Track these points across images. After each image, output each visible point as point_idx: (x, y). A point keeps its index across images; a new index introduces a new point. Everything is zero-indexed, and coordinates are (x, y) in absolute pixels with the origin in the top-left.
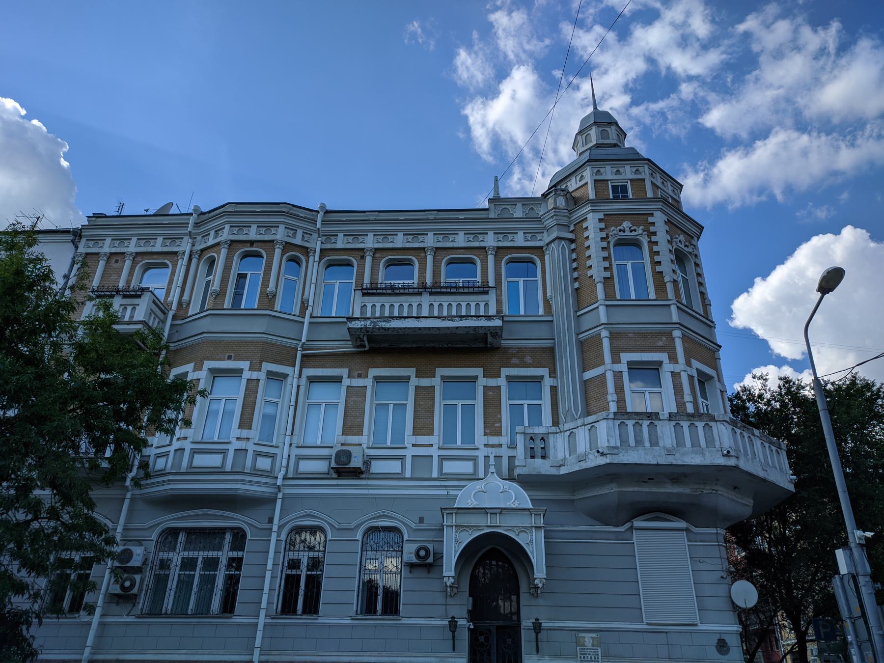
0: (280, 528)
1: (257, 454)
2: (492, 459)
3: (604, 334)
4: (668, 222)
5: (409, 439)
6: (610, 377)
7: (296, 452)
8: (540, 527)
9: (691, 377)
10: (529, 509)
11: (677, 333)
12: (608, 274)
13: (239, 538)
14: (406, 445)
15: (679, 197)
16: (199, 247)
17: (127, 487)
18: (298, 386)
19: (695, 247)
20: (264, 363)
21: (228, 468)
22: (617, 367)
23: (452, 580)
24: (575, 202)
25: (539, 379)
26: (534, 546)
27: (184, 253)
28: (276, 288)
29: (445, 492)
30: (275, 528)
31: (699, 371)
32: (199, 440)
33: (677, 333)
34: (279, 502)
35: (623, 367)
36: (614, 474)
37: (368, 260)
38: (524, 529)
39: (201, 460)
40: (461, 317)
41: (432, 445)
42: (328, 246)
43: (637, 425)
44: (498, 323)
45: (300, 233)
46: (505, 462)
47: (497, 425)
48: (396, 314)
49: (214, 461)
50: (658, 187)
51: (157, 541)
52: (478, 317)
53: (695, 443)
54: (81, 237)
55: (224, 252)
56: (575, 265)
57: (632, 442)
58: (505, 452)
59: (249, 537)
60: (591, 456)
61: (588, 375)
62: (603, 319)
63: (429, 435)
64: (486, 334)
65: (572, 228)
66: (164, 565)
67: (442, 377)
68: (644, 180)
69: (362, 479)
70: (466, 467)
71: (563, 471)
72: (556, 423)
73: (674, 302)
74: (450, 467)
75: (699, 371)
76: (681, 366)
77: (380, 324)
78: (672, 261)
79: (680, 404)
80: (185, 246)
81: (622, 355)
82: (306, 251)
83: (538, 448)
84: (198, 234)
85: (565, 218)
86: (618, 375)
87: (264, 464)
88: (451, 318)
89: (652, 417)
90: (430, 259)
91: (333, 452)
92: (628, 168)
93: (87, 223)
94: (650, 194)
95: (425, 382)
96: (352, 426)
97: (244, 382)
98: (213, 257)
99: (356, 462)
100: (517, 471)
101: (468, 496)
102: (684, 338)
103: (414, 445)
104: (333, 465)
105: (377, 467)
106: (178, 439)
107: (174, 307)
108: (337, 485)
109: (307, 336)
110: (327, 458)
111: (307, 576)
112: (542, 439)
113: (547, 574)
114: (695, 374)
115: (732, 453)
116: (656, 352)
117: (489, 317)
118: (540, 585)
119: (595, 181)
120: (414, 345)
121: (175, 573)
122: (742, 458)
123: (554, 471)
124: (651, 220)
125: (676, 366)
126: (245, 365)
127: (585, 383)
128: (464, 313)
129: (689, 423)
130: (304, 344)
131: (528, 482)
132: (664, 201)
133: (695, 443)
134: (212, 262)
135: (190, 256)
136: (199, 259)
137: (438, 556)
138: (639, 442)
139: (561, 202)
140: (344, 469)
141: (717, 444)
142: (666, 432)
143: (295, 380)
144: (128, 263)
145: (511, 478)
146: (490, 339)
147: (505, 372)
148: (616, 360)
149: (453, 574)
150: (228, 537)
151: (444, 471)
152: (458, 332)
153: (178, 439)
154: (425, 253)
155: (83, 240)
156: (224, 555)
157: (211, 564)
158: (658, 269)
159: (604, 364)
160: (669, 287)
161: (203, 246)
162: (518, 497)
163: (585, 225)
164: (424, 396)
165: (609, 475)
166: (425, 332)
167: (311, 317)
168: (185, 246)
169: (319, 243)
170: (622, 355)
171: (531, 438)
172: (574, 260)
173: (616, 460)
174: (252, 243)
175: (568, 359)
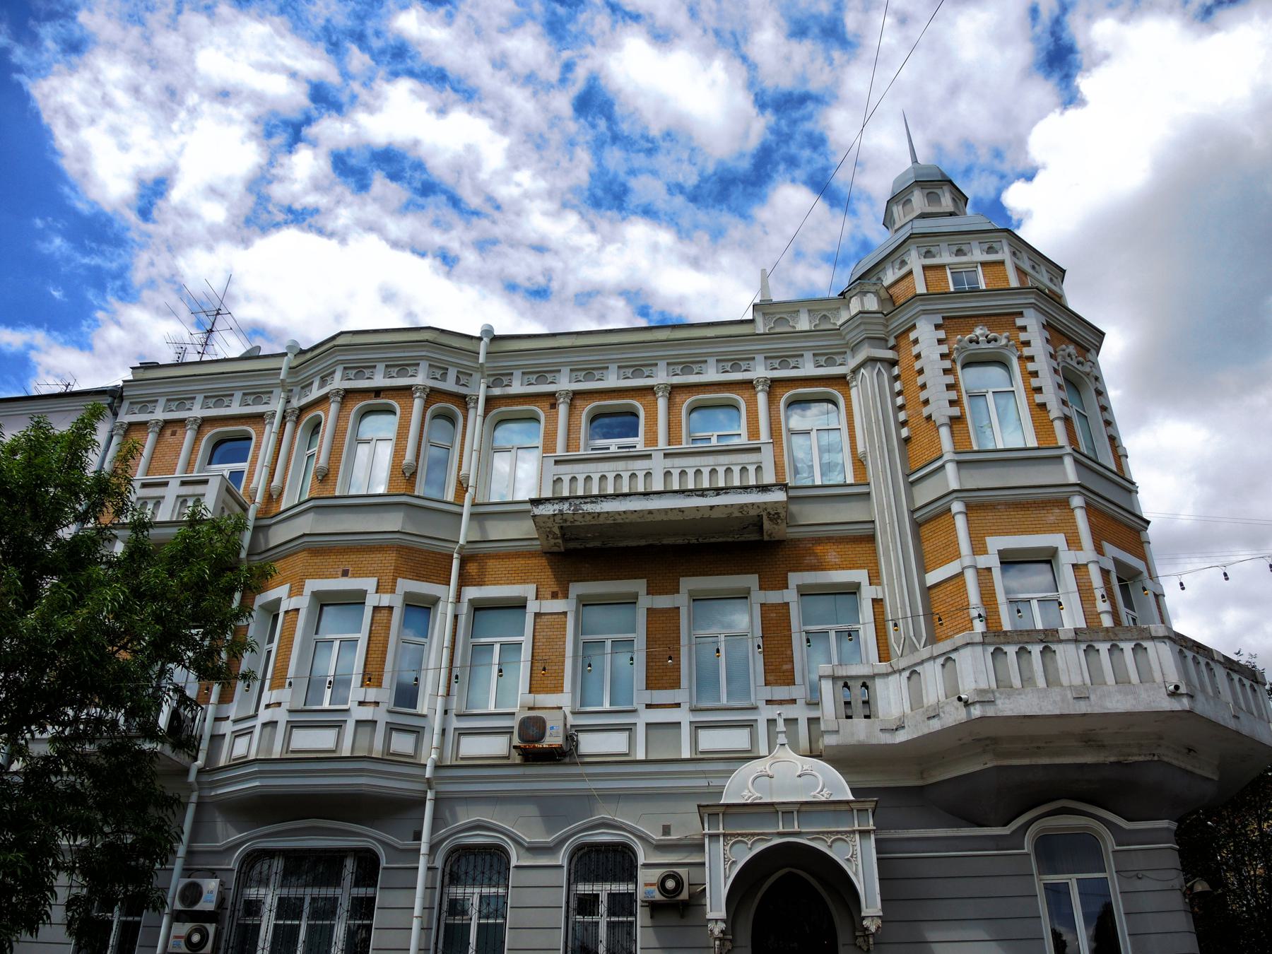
0: (433, 848)
1: (392, 728)
2: (781, 726)
3: (957, 507)
4: (1047, 326)
5: (642, 696)
6: (970, 576)
7: (455, 723)
8: (868, 832)
9: (1105, 573)
10: (848, 802)
11: (1077, 501)
12: (955, 411)
13: (368, 868)
14: (635, 706)
15: (1061, 289)
16: (296, 403)
17: (190, 784)
18: (456, 617)
19: (1095, 364)
20: (399, 580)
21: (346, 752)
22: (982, 562)
23: (723, 926)
24: (891, 304)
25: (852, 590)
26: (860, 862)
27: (274, 414)
28: (417, 461)
29: (704, 783)
30: (424, 848)
31: (1115, 560)
32: (301, 706)
33: (1077, 501)
34: (429, 807)
35: (992, 561)
36: (987, 738)
37: (562, 409)
38: (840, 837)
39: (307, 740)
40: (718, 491)
41: (678, 705)
42: (497, 391)
43: (1022, 652)
44: (780, 496)
45: (452, 373)
46: (803, 727)
47: (785, 667)
48: (610, 491)
49: (321, 740)
50: (1026, 274)
51: (239, 872)
52: (745, 488)
53: (1121, 679)
54: (121, 398)
55: (334, 408)
56: (900, 401)
57: (1017, 682)
58: (801, 713)
59: (383, 863)
60: (947, 708)
61: (932, 578)
62: (954, 485)
63: (673, 688)
64: (760, 517)
65: (892, 342)
66: (253, 908)
67: (691, 593)
68: (1002, 263)
69: (565, 764)
70: (737, 740)
71: (901, 737)
72: (884, 655)
73: (1068, 449)
74: (712, 740)
75: (1115, 560)
76: (1087, 554)
77: (585, 507)
78: (1060, 387)
79: (1091, 615)
80: (277, 405)
81: (989, 540)
82: (463, 401)
83: (858, 697)
84: (295, 384)
85: (881, 328)
86: (984, 574)
87: (403, 743)
88: (701, 492)
89: (1048, 638)
90: (662, 403)
91: (514, 723)
92: (975, 244)
93: (131, 378)
94: (1014, 283)
95: (663, 602)
96: (544, 676)
97: (368, 612)
98: (319, 416)
99: (553, 739)
100: (830, 740)
101: (741, 786)
102: (1089, 508)
103: (649, 706)
104: (516, 741)
105: (589, 744)
106: (268, 706)
107: (259, 498)
108: (524, 776)
109: (466, 535)
110: (507, 731)
111: (479, 925)
112: (864, 685)
113: (883, 909)
114: (1110, 566)
115: (1183, 690)
116: (1045, 532)
117: (764, 488)
118: (873, 929)
119: (925, 268)
120: (643, 543)
121: (267, 923)
122: (1200, 697)
123: (887, 739)
124: (1020, 322)
125: (1079, 552)
126: (369, 584)
127: (927, 591)
128: (721, 484)
129: (1108, 645)
130: (462, 547)
131: (843, 760)
132: (1039, 291)
133: (1121, 679)
134: (316, 427)
135: (284, 417)
136: (297, 423)
137: (698, 897)
138: (1027, 680)
139: (872, 303)
140: (537, 750)
141: (1158, 676)
142: (1069, 658)
143: (450, 607)
144: (190, 435)
145: (813, 754)
146: (767, 525)
147: (795, 579)
148: (978, 548)
149: (722, 914)
150: (350, 865)
151: (701, 748)
152: (715, 514)
153: (268, 706)
154: (655, 394)
155: (126, 404)
156: (345, 893)
157: (326, 910)
158: (1039, 399)
159: (959, 556)
160: (1059, 427)
161: (304, 401)
162: (830, 784)
163: (912, 336)
164: (663, 632)
165: (979, 740)
166: (658, 518)
167: (474, 505)
168: (277, 405)
169: (483, 387)
170: (989, 540)
171: (846, 685)
172: (900, 393)
173: (990, 711)
174: (378, 392)
175: (893, 546)
